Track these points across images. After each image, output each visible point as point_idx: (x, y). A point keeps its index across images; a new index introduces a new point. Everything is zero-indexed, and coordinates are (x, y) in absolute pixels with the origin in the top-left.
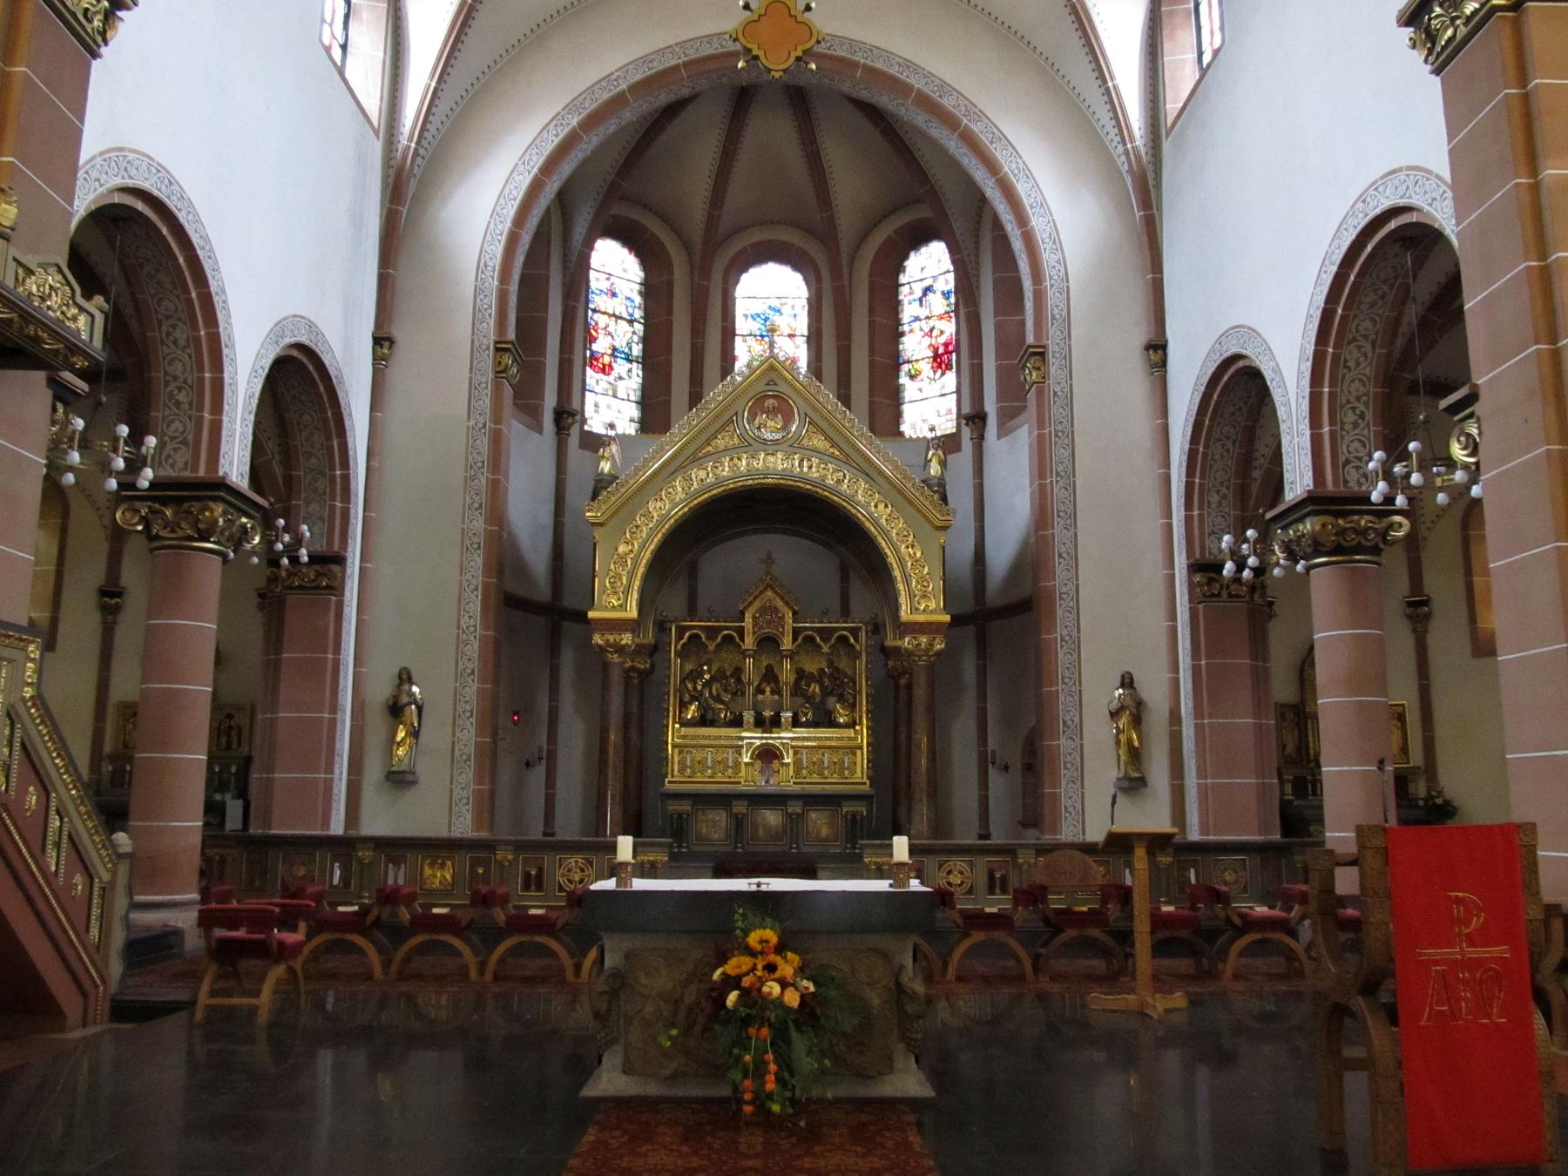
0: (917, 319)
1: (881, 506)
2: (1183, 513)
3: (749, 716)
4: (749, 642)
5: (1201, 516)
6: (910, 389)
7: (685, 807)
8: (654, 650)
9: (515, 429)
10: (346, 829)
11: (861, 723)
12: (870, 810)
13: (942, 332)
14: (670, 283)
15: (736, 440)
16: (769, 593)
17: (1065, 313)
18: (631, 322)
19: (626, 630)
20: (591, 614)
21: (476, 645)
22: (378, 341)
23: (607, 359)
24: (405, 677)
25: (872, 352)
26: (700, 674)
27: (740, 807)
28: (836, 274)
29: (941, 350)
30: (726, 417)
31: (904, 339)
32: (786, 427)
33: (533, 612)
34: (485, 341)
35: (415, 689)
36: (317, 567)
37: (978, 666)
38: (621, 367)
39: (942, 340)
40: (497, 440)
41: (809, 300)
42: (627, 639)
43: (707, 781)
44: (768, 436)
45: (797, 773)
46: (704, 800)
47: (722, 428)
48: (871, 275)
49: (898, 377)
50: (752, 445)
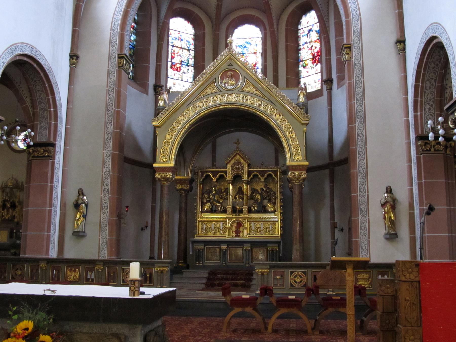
0: (306, 43)
1: (278, 116)
2: (413, 114)
3: (230, 209)
4: (229, 177)
5: (421, 115)
6: (304, 72)
7: (201, 246)
8: (191, 181)
9: (131, 92)
10: (58, 255)
11: (278, 211)
12: (279, 248)
13: (316, 48)
14: (204, 34)
15: (215, 90)
16: (238, 156)
17: (359, 29)
18: (189, 50)
19: (169, 172)
20: (155, 165)
21: (109, 179)
22: (71, 57)
23: (178, 66)
24: (81, 193)
25: (287, 57)
26: (211, 191)
27: (224, 247)
28: (271, 26)
29: (316, 55)
30: (211, 80)
31: (301, 52)
32: (236, 83)
33: (132, 163)
34: (114, 55)
35: (85, 198)
36: (44, 148)
37: (330, 186)
38: (184, 68)
39: (316, 51)
40: (119, 94)
41: (262, 38)
42: (169, 175)
43: (210, 236)
44: (229, 87)
45: (250, 232)
46: (207, 243)
47: (210, 85)
48: (286, 26)
49: (298, 67)
50: (220, 91)
